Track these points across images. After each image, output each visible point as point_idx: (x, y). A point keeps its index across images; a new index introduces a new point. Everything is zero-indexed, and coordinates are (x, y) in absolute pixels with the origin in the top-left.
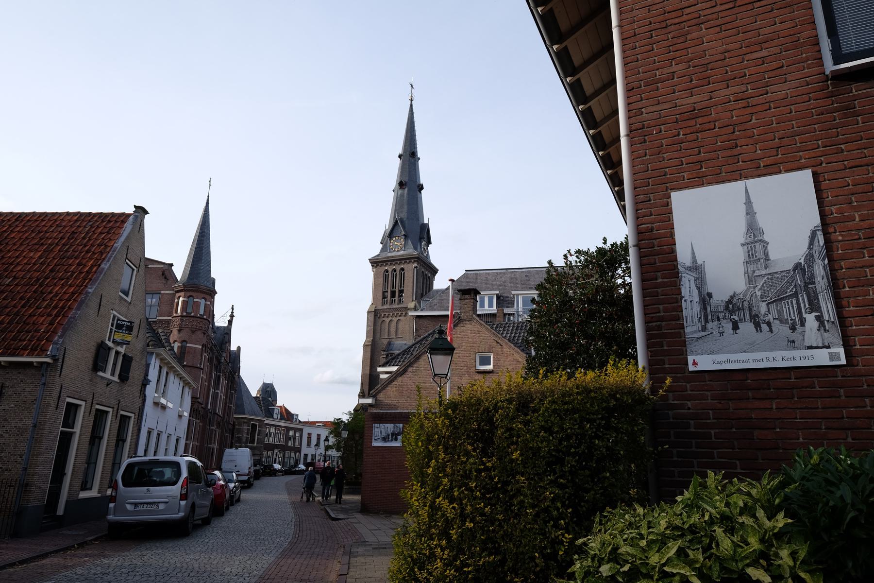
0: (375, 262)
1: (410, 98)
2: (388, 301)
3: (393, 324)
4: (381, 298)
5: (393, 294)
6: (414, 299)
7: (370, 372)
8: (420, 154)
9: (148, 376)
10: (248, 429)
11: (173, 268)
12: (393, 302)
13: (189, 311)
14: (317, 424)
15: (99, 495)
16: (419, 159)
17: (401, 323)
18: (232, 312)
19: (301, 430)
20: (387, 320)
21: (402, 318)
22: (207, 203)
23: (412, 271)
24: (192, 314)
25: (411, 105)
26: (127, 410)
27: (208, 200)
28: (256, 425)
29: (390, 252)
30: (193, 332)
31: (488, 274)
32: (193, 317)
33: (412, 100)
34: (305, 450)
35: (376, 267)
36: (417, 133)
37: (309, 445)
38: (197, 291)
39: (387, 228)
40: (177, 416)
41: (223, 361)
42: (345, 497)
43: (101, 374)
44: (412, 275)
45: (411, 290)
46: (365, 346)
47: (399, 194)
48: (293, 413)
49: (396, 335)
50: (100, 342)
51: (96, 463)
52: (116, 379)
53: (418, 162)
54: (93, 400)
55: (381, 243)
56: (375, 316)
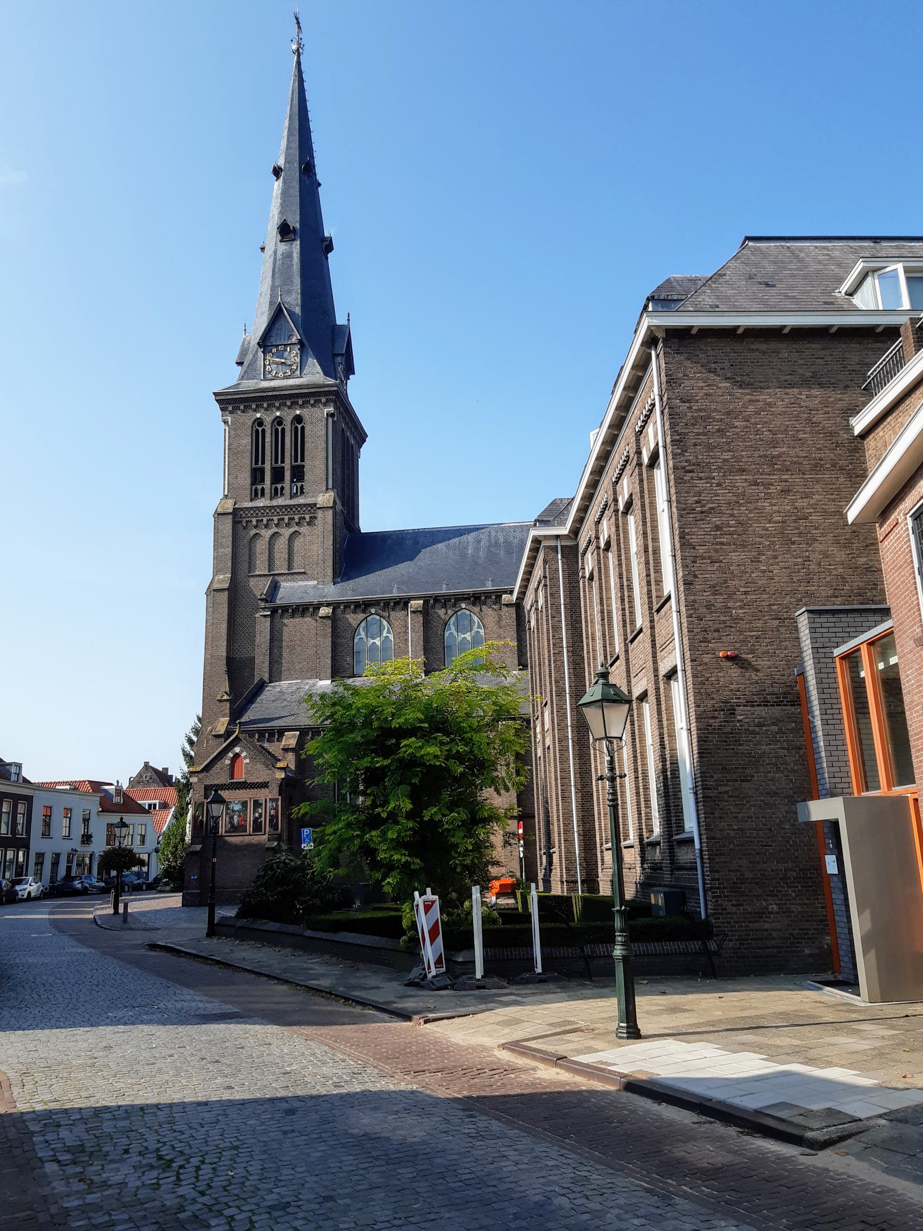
1: (294, 47)
2: (267, 491)
3: (281, 545)
4: (249, 481)
5: (278, 475)
6: (330, 486)
7: (228, 652)
12: (276, 494)
16: (320, 185)
17: (298, 543)
19: (29, 800)
20: (267, 534)
21: (304, 529)
23: (324, 423)
25: (299, 63)
29: (265, 379)
37: (46, 834)
40: (58, 852)
44: (324, 432)
45: (323, 467)
46: (212, 591)
47: (279, 253)
48: (7, 760)
49: (289, 568)
55: (240, 364)
56: (235, 523)
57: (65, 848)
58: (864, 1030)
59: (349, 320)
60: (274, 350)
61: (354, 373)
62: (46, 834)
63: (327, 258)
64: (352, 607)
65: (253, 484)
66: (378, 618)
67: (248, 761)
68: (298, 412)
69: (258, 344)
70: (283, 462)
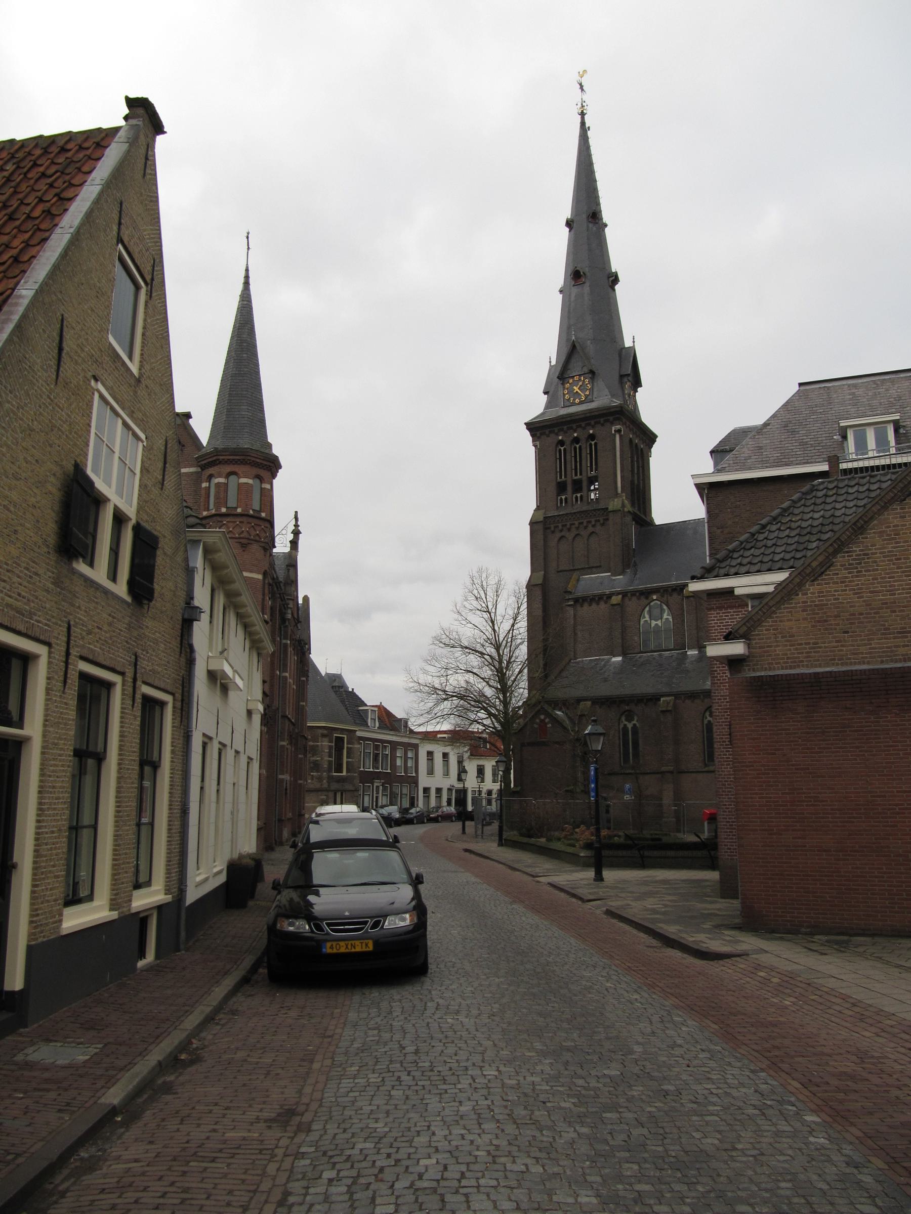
0: (535, 428)
8: (607, 214)
9: (192, 598)
10: (330, 747)
11: (191, 422)
13: (232, 503)
14: (439, 736)
15: (114, 915)
16: (606, 225)
18: (296, 526)
19: (415, 747)
22: (247, 283)
24: (239, 510)
26: (156, 683)
27: (247, 277)
28: (342, 739)
30: (244, 546)
31: (855, 386)
32: (241, 515)
33: (582, 114)
34: (424, 781)
35: (539, 438)
36: (598, 176)
37: (431, 772)
38: (243, 462)
39: (554, 363)
40: (245, 711)
41: (289, 616)
42: (606, 873)
43: (81, 567)
50: (71, 468)
51: (95, 827)
52: (121, 589)
53: (604, 230)
54: (68, 643)
55: (545, 393)
56: (546, 529)
57: (445, 784)
58: (743, 942)
59: (634, 342)
60: (571, 381)
61: (641, 386)
62: (431, 772)
63: (614, 290)
64: (638, 594)
65: (558, 495)
66: (659, 603)
67: (549, 725)
68: (591, 432)
69: (558, 377)
70: (581, 474)
